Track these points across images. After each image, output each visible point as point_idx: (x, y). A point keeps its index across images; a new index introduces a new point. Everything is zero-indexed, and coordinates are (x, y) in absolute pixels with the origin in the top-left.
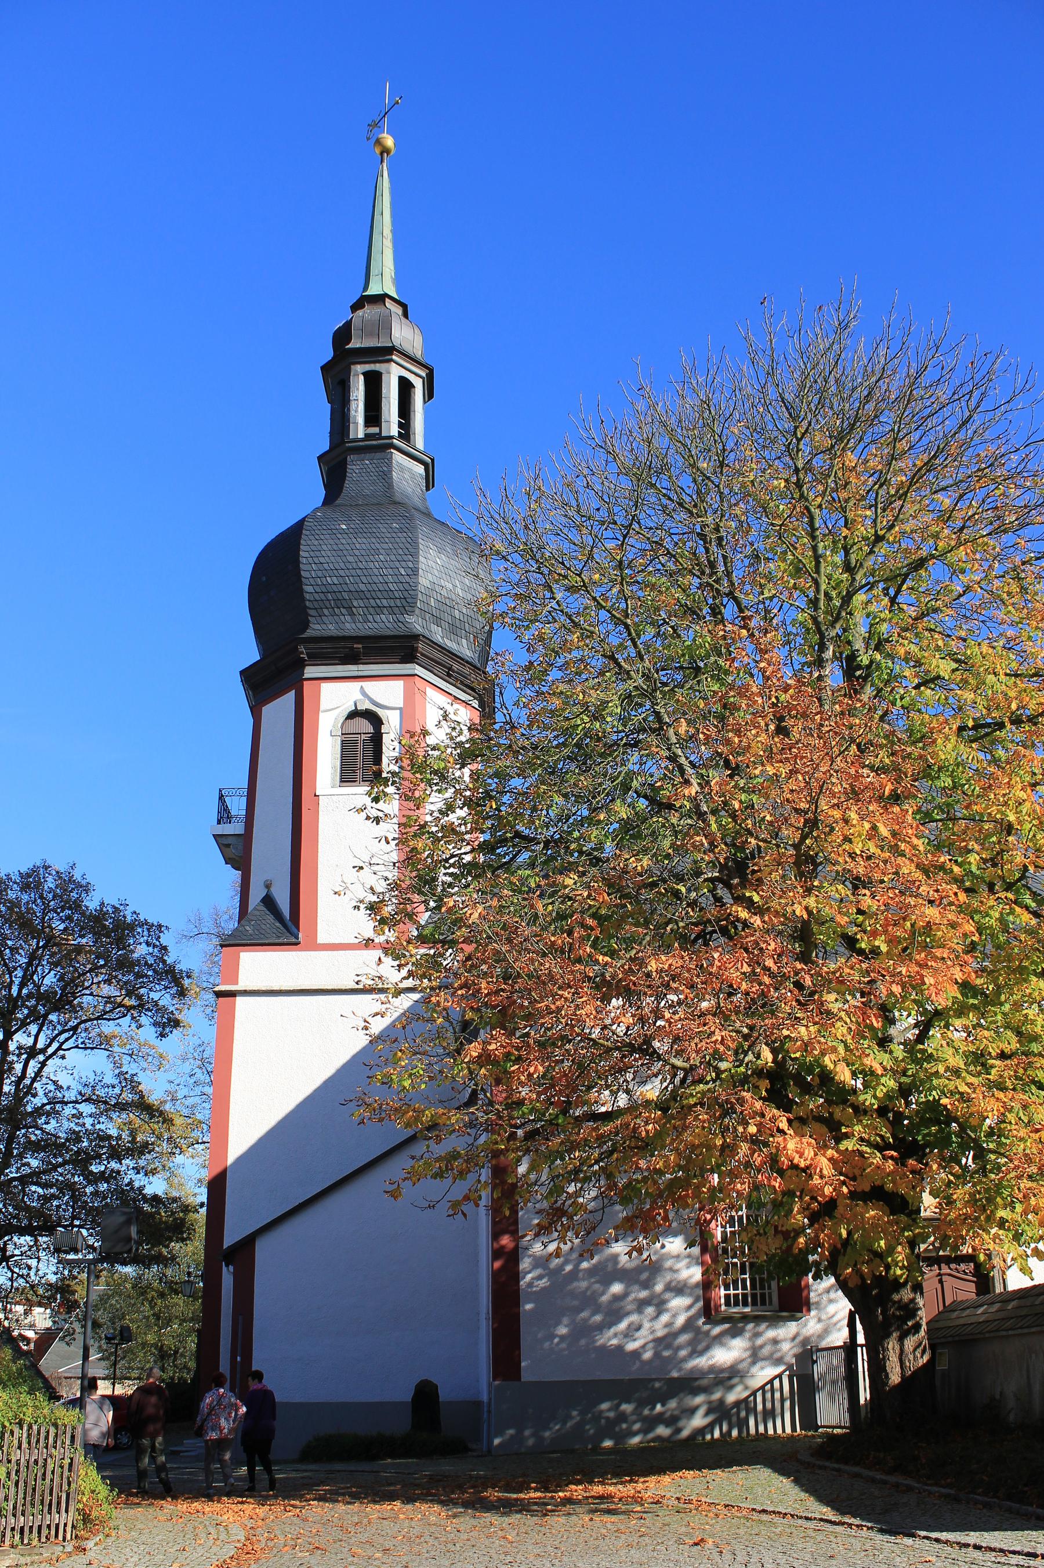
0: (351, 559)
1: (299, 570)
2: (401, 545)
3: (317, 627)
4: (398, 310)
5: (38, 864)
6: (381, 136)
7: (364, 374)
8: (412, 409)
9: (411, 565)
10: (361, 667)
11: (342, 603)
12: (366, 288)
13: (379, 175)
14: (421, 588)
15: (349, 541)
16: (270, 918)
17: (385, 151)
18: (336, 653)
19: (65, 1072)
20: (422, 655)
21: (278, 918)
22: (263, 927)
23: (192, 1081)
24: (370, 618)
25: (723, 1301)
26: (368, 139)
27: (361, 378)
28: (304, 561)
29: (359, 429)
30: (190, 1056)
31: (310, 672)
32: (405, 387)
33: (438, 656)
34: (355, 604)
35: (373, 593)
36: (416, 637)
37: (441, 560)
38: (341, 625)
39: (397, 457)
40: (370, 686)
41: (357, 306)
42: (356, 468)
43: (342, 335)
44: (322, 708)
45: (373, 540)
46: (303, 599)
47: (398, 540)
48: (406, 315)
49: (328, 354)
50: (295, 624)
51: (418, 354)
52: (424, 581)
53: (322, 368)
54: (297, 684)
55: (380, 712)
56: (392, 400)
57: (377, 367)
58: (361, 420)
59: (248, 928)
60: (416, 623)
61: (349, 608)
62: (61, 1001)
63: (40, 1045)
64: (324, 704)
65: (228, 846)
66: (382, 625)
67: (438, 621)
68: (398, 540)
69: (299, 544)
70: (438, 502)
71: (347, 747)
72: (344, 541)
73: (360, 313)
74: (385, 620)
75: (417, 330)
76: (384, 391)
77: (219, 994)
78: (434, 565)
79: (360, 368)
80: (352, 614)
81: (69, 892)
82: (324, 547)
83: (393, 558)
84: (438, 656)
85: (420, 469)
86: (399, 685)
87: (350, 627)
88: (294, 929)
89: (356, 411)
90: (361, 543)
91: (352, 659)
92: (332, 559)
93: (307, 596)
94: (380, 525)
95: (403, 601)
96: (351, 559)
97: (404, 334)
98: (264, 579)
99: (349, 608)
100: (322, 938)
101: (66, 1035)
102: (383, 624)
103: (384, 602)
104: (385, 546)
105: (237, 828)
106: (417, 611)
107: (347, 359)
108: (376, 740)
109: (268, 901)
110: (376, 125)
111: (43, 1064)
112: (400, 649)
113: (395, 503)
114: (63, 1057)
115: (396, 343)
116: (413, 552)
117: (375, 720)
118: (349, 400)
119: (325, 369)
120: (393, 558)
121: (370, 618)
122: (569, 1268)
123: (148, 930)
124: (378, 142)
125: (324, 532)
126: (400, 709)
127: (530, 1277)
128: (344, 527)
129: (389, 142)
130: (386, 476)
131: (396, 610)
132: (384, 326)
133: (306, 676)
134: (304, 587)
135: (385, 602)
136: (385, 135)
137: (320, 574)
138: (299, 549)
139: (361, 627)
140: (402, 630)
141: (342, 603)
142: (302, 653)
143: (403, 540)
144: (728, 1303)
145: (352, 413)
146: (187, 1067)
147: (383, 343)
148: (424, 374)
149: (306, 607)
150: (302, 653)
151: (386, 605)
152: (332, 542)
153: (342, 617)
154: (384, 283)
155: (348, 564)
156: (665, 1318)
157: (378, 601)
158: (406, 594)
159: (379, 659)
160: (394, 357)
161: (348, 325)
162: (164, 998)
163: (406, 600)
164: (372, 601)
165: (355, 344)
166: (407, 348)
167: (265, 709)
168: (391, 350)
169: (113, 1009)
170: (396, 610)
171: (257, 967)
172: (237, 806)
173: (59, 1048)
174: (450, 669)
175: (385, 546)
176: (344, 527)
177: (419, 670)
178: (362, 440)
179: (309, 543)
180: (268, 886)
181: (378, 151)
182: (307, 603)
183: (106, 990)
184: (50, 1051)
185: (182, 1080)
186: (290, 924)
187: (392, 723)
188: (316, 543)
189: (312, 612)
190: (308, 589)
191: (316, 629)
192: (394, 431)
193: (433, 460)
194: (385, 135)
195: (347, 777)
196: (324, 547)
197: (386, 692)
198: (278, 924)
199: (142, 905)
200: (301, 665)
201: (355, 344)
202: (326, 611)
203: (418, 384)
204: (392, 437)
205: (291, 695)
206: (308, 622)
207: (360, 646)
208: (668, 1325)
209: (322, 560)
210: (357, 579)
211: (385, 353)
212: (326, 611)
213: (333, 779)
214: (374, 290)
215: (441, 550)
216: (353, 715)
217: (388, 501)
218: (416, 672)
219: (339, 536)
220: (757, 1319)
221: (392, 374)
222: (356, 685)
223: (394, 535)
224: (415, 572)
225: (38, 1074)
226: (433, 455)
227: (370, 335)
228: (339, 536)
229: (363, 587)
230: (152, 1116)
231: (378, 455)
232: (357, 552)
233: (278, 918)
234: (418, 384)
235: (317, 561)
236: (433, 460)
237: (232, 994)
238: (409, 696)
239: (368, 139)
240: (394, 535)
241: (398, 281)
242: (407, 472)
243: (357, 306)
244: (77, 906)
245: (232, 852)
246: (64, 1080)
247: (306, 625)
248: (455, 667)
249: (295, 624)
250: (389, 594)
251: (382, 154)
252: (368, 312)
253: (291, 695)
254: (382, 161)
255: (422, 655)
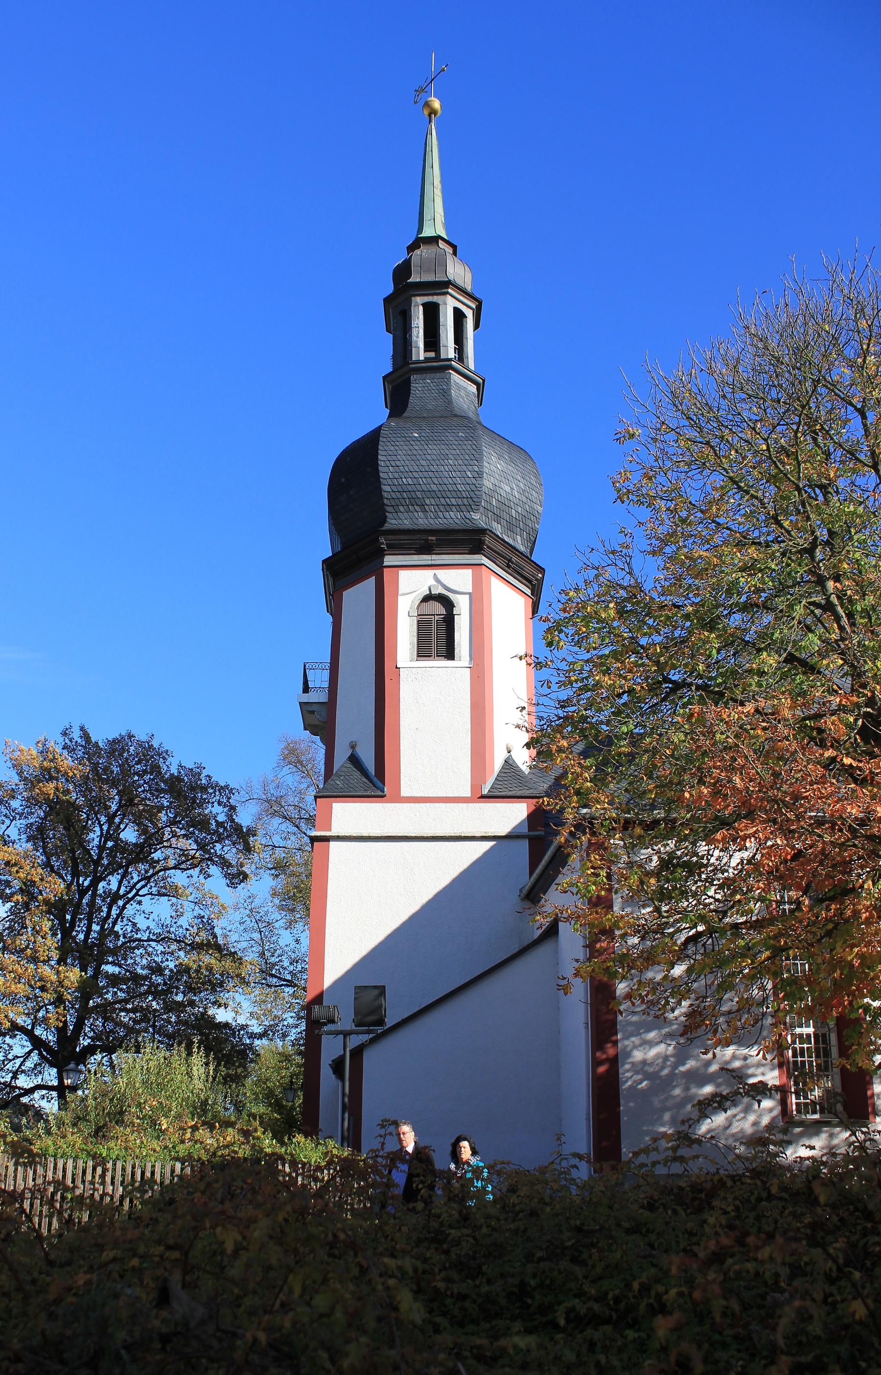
0: (423, 463)
1: (378, 472)
2: (468, 452)
3: (394, 522)
4: (449, 250)
5: (123, 734)
6: (429, 99)
7: (423, 305)
8: (465, 336)
9: (476, 469)
10: (434, 557)
11: (416, 502)
12: (420, 230)
13: (428, 133)
14: (484, 489)
15: (421, 447)
16: (357, 774)
17: (433, 112)
18: (412, 544)
19: (143, 915)
20: (488, 547)
21: (371, 775)
22: (352, 781)
23: (242, 928)
24: (441, 514)
25: (794, 1107)
26: (415, 103)
27: (421, 308)
28: (382, 464)
29: (420, 352)
30: (240, 905)
31: (389, 560)
32: (459, 316)
33: (500, 548)
34: (427, 502)
35: (443, 493)
36: (483, 531)
37: (501, 465)
38: (415, 521)
39: (455, 377)
40: (442, 574)
41: (412, 248)
42: (420, 387)
43: (402, 272)
44: (400, 592)
45: (443, 447)
46: (382, 497)
47: (464, 447)
48: (455, 253)
49: (390, 289)
50: (365, 525)
51: (469, 288)
52: (487, 483)
53: (384, 300)
54: (378, 573)
55: (451, 596)
56: (449, 328)
57: (435, 299)
58: (421, 345)
59: (338, 782)
60: (478, 519)
61: (422, 506)
62: (140, 853)
63: (122, 892)
64: (402, 589)
65: (313, 712)
66: (451, 521)
67: (498, 518)
68: (464, 447)
69: (377, 449)
70: (487, 416)
71: (423, 627)
72: (416, 447)
73: (418, 252)
74: (453, 516)
75: (467, 268)
76: (441, 320)
77: (314, 839)
78: (495, 469)
79: (419, 300)
80: (424, 511)
81: (151, 756)
82: (400, 452)
83: (461, 462)
84: (500, 548)
85: (473, 388)
86: (468, 573)
87: (422, 521)
88: (379, 784)
89: (418, 337)
90: (433, 450)
91: (426, 549)
92: (407, 462)
93: (385, 495)
94: (448, 434)
95: (470, 500)
96: (423, 463)
97: (457, 271)
98: (343, 480)
99: (422, 506)
100: (405, 792)
101: (143, 883)
102: (452, 519)
103: (453, 501)
104: (454, 452)
105: (317, 697)
106: (482, 509)
107: (407, 293)
108: (449, 621)
109: (354, 760)
110: (421, 90)
111: (124, 907)
112: (469, 541)
113: (456, 416)
114: (140, 903)
115: (451, 278)
116: (477, 457)
117: (448, 604)
118: (411, 328)
119: (387, 301)
120: (461, 462)
121: (441, 514)
122: (666, 1072)
123: (219, 790)
124: (427, 104)
125: (399, 439)
126: (469, 594)
127: (628, 1078)
128: (416, 435)
129: (437, 104)
130: (445, 393)
131: (463, 508)
132: (440, 263)
133: (385, 564)
134: (383, 487)
135: (454, 501)
136: (432, 98)
137: (396, 475)
138: (377, 454)
139: (432, 522)
140: (469, 525)
141: (416, 502)
142: (383, 544)
143: (469, 447)
144: (799, 1111)
145: (414, 338)
146: (237, 916)
147: (440, 278)
148: (474, 306)
149: (384, 504)
150: (383, 544)
151: (455, 503)
152: (406, 448)
153: (416, 514)
154: (435, 226)
155: (421, 467)
156: (752, 1118)
157: (447, 500)
158: (472, 494)
159: (449, 550)
160: (450, 290)
161: (407, 264)
162: (229, 851)
163: (472, 501)
164: (442, 500)
165: (414, 278)
166: (460, 282)
167: (346, 594)
168: (448, 284)
169: (185, 862)
170: (463, 508)
171: (346, 816)
172: (320, 679)
173: (137, 894)
174: (510, 561)
175: (454, 452)
176: (416, 435)
177: (485, 561)
178: (422, 362)
179: (386, 448)
180: (353, 747)
181: (426, 112)
182: (385, 501)
183: (183, 843)
184: (130, 896)
185: (233, 927)
186: (375, 780)
187: (462, 605)
188: (392, 448)
189: (389, 509)
190: (386, 488)
191: (392, 522)
192: (451, 354)
193: (484, 381)
194: (432, 98)
195: (423, 652)
196: (400, 452)
197: (457, 580)
198: (364, 780)
199: (218, 772)
200: (381, 554)
201: (414, 278)
202: (401, 508)
203: (469, 314)
204: (450, 360)
205: (372, 580)
206: (386, 517)
207: (434, 538)
208: (755, 1124)
209: (398, 463)
210: (429, 480)
211: (443, 286)
212: (401, 508)
213: (411, 654)
214: (428, 232)
215: (500, 457)
216: (428, 598)
217: (448, 416)
218: (483, 562)
219: (412, 443)
220: (827, 1124)
221: (448, 305)
222: (429, 573)
223: (461, 443)
224: (480, 475)
225: (120, 915)
226: (484, 376)
227: (428, 270)
228: (412, 443)
229: (434, 488)
230: (223, 956)
231: (438, 375)
232: (429, 457)
233: (371, 775)
234: (469, 314)
235: (396, 465)
236: (484, 381)
237: (327, 839)
238: (477, 583)
239: (415, 103)
240: (461, 443)
241: (447, 225)
242: (462, 390)
243: (412, 248)
244: (156, 769)
245: (314, 720)
246: (142, 923)
247: (384, 520)
248: (514, 559)
249: (365, 525)
250: (458, 494)
251: (430, 115)
252: (423, 252)
253: (372, 580)
254: (430, 121)
255: (488, 547)
